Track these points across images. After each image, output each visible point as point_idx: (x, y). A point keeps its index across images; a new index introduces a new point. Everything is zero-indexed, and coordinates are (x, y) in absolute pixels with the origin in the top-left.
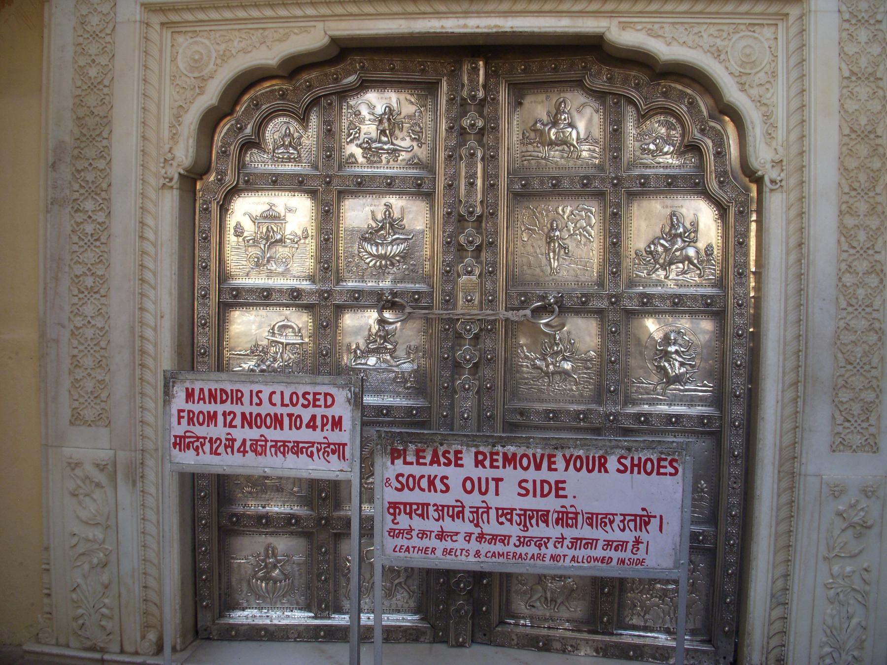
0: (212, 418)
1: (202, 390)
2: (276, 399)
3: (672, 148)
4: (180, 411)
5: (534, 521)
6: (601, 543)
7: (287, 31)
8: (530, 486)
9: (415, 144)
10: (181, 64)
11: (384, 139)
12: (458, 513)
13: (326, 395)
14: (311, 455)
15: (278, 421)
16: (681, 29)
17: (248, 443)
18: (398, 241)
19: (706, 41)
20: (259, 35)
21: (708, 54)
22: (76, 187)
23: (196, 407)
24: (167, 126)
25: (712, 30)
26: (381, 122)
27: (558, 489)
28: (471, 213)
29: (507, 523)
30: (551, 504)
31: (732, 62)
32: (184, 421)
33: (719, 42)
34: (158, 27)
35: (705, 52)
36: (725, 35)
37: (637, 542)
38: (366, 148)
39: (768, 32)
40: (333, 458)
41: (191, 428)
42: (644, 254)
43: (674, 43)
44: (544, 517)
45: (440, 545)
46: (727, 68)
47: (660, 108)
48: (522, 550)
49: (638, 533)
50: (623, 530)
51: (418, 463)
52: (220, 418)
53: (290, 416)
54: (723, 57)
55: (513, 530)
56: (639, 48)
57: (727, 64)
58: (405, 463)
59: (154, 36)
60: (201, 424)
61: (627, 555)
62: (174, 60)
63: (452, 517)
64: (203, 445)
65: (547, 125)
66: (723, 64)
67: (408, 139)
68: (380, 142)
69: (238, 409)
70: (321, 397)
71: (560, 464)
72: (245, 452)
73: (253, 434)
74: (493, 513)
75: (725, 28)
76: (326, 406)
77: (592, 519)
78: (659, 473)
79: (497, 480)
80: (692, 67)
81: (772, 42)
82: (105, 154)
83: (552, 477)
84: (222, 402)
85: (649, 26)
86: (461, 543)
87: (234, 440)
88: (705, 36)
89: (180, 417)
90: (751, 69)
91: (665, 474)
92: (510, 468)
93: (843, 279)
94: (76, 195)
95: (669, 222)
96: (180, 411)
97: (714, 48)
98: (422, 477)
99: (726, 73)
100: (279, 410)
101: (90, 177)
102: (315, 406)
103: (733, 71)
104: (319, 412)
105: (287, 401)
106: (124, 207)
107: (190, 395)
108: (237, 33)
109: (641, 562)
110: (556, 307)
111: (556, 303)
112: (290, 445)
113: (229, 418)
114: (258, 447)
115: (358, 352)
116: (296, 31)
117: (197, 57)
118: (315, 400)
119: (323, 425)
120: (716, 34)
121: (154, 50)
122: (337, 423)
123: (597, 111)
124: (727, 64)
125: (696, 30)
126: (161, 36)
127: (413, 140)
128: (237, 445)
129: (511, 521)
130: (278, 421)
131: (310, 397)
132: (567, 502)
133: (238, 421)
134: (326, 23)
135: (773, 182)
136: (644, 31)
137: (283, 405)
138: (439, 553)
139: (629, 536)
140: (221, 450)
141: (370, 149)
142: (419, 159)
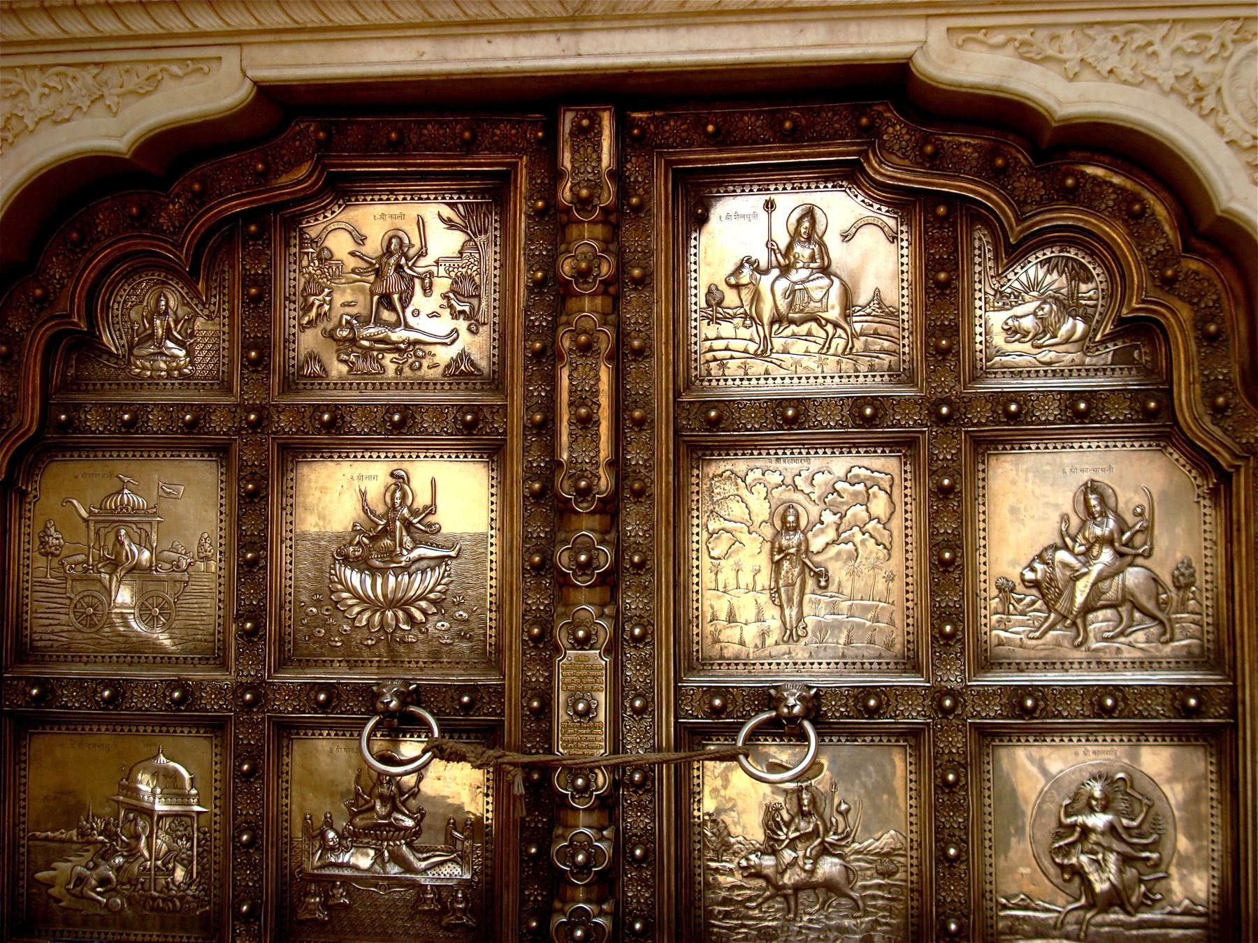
3: (1081, 326)
7: (153, 69)
9: (462, 325)
11: (386, 315)
16: (1102, 38)
18: (424, 564)
19: (1166, 67)
20: (89, 79)
21: (1173, 97)
25: (1181, 37)
26: (379, 273)
28: (584, 494)
31: (1234, 114)
33: (1199, 67)
35: (1166, 94)
36: (1213, 48)
38: (345, 339)
42: (1020, 588)
43: (1087, 74)
46: (1220, 130)
47: (1119, 264)
54: (1209, 103)
56: (998, 89)
57: (1222, 119)
65: (766, 272)
66: (1211, 119)
67: (446, 313)
68: (379, 322)
75: (1213, 31)
80: (1206, 192)
85: (1026, 36)
88: (1164, 53)
95: (1081, 508)
97: (1189, 81)
99: (1220, 142)
103: (1236, 135)
108: (36, 75)
110: (807, 724)
111: (806, 715)
115: (331, 835)
116: (175, 69)
117: (1139, 510)
120: (1191, 46)
123: (893, 239)
124: (1222, 119)
125: (1139, 39)
127: (455, 315)
134: (246, 50)
136: (1010, 49)
141: (353, 341)
142: (473, 364)
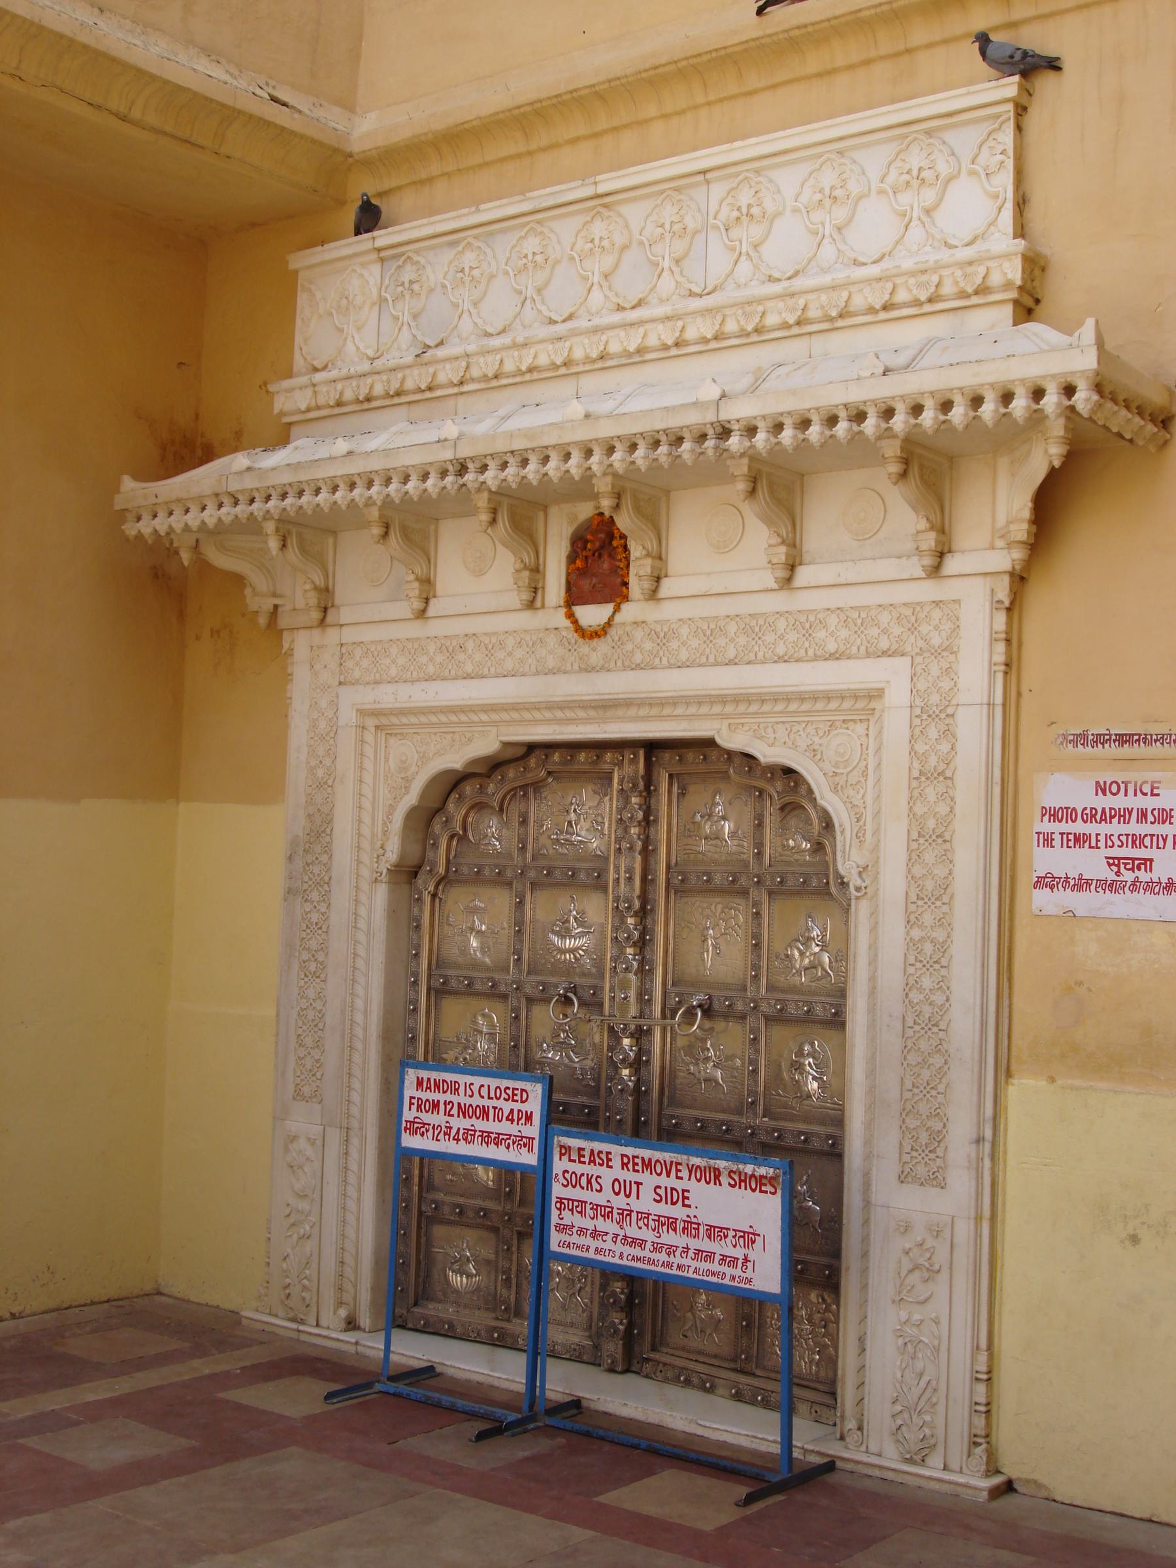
0: (435, 1105)
1: (429, 1080)
2: (484, 1092)
4: (411, 1098)
5: (665, 1228)
6: (717, 1257)
8: (662, 1192)
10: (392, 764)
12: (606, 1212)
13: (522, 1090)
14: (508, 1148)
15: (485, 1112)
17: (462, 1131)
22: (306, 879)
23: (425, 1095)
24: (380, 822)
27: (684, 1198)
29: (644, 1228)
30: (678, 1212)
32: (414, 1108)
34: (373, 730)
37: (746, 1260)
39: (860, 728)
40: (524, 1150)
41: (419, 1114)
44: (671, 1223)
45: (594, 1244)
48: (655, 1256)
49: (746, 1251)
50: (735, 1246)
51: (580, 1162)
52: (442, 1107)
53: (495, 1108)
55: (648, 1235)
58: (570, 1160)
59: (369, 737)
60: (427, 1112)
61: (737, 1272)
62: (387, 759)
63: (603, 1216)
64: (427, 1131)
69: (455, 1099)
70: (518, 1092)
71: (685, 1173)
72: (458, 1140)
73: (465, 1123)
74: (634, 1215)
76: (522, 1102)
77: (715, 1232)
78: (761, 1191)
79: (638, 1184)
81: (864, 739)
82: (328, 850)
83: (680, 1185)
84: (444, 1092)
86: (609, 1245)
87: (451, 1128)
89: (411, 1104)
90: (845, 768)
91: (766, 1192)
92: (647, 1173)
93: (910, 995)
94: (306, 886)
96: (411, 1098)
98: (582, 1175)
100: (486, 1102)
101: (316, 870)
102: (513, 1101)
104: (517, 1106)
105: (492, 1095)
106: (341, 897)
107: (420, 1083)
109: (750, 1281)
112: (493, 1136)
113: (449, 1107)
114: (468, 1135)
118: (514, 1095)
119: (519, 1119)
121: (369, 751)
122: (529, 1118)
126: (376, 738)
128: (453, 1132)
129: (647, 1225)
130: (485, 1112)
131: (510, 1092)
132: (691, 1212)
133: (455, 1111)
135: (858, 889)
137: (490, 1098)
138: (592, 1250)
139: (739, 1253)
140: (441, 1136)
